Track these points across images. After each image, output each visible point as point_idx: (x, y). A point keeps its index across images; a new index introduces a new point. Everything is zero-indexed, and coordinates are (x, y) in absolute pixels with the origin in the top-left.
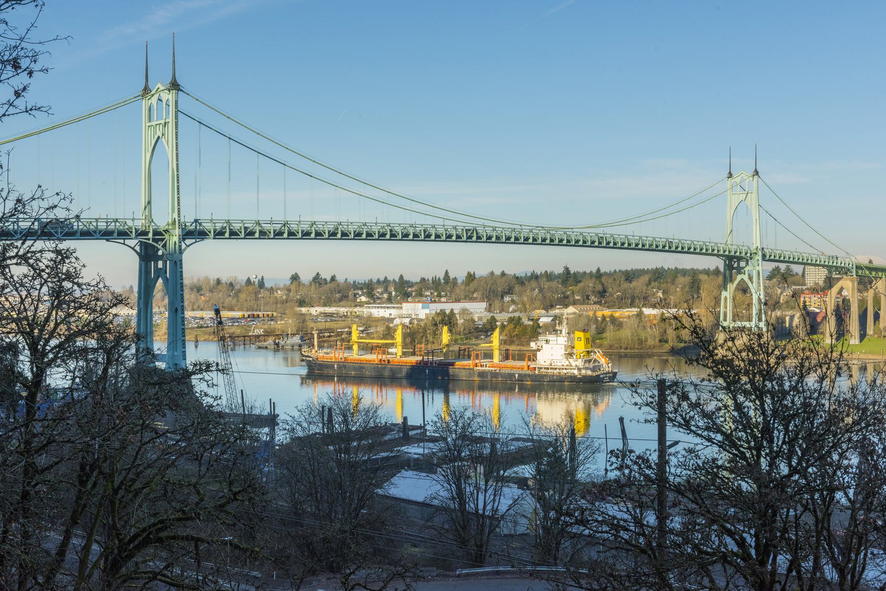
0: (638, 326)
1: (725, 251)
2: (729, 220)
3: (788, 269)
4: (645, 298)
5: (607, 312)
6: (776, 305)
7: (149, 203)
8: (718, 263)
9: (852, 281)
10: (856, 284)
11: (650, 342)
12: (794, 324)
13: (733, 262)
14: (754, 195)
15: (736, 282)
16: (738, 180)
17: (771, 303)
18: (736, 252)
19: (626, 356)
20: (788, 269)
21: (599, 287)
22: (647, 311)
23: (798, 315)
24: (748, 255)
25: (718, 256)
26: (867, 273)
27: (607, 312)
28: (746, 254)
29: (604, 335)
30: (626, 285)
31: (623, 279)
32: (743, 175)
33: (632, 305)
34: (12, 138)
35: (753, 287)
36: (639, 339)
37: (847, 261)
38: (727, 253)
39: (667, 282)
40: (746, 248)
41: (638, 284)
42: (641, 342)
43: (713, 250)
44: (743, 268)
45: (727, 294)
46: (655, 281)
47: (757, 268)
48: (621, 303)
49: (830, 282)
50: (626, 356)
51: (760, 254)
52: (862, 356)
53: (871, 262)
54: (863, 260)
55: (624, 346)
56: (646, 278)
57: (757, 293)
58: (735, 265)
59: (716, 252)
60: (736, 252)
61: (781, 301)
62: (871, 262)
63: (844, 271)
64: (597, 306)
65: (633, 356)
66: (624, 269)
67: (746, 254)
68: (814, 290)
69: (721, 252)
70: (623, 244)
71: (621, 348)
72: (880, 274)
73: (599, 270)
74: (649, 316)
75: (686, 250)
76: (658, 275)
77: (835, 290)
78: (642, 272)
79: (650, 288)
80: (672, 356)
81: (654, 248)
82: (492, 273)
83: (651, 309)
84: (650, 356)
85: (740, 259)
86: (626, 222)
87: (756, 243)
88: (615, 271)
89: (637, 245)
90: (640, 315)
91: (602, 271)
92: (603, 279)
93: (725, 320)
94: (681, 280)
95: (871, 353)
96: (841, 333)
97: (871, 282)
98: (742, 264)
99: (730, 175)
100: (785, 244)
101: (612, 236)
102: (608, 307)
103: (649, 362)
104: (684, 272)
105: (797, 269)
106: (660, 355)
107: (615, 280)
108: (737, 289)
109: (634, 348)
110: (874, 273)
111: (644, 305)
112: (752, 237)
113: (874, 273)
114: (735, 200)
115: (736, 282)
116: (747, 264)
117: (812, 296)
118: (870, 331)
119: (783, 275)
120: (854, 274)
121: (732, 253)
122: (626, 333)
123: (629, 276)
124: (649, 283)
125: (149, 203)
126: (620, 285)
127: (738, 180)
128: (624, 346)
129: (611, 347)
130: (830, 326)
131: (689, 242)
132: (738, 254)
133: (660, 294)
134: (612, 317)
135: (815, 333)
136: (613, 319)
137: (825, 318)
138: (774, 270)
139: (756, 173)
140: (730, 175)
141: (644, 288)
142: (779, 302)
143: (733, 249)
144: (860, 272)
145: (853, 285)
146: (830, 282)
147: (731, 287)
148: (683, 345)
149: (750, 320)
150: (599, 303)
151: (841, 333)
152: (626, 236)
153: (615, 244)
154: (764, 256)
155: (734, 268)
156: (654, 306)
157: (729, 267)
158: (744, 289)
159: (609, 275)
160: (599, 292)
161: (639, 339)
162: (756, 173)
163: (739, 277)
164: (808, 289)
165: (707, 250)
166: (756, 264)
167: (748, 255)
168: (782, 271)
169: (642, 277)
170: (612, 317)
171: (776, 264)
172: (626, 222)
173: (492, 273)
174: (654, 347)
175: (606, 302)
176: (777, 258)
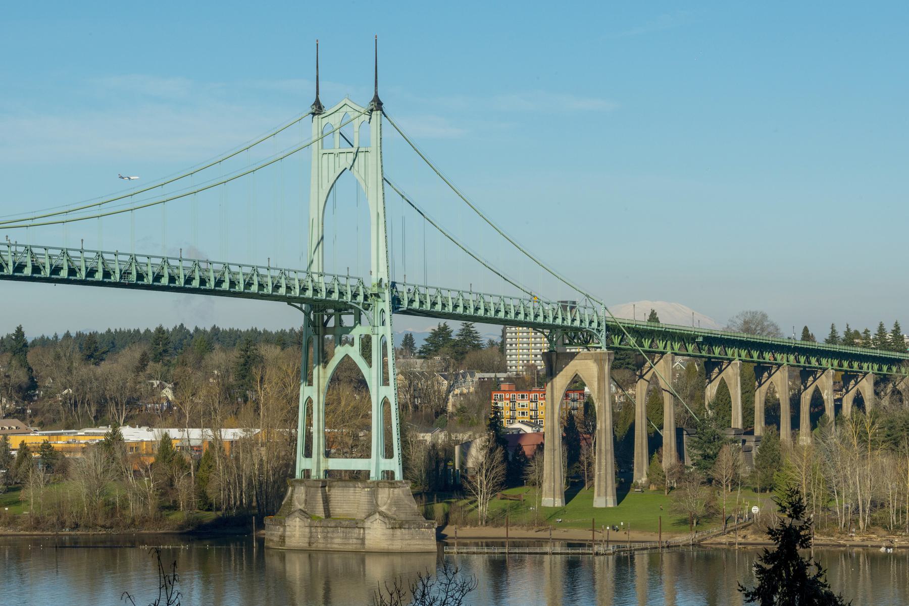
0: (106, 471)
1: (304, 290)
2: (314, 213)
3: (467, 333)
4: (132, 402)
5: (36, 438)
6: (436, 416)
7: (322, 238)
8: (290, 319)
9: (598, 360)
10: (607, 368)
11: (134, 509)
12: (470, 464)
13: (326, 314)
14: (372, 159)
15: (333, 363)
16: (335, 120)
17: (420, 410)
18: (330, 292)
19: (75, 544)
20: (467, 333)
21: (21, 376)
22: (131, 434)
23: (478, 442)
24: (360, 299)
25: (290, 300)
26: (632, 341)
27: (36, 438)
28: (355, 296)
29: (22, 495)
30: (85, 371)
31: (77, 356)
32: (347, 107)
33: (99, 420)
34: (246, 171)
35: (371, 375)
36: (107, 504)
37: (587, 314)
38: (309, 294)
39: (184, 364)
40: (354, 282)
41: (116, 370)
42: (111, 509)
43: (277, 287)
44: (348, 330)
45: (313, 392)
46: (156, 360)
47: (381, 330)
48: (72, 415)
49: (554, 361)
50: (75, 544)
51: (387, 296)
52: (620, 536)
53: (653, 317)
54: (632, 312)
55: (69, 521)
56: (130, 356)
57: (383, 392)
58: (331, 323)
59: (282, 291)
60: (330, 292)
61: (450, 408)
62: (653, 317)
63: (580, 336)
64: (14, 423)
65: (92, 545)
66: (86, 329)
67: (355, 296)
68: (520, 384)
69: (296, 292)
70: (56, 270)
71: (63, 525)
72: (661, 345)
73: (20, 333)
74: (138, 444)
75: (240, 287)
76: (164, 347)
77: (561, 381)
78: (133, 337)
79: (142, 377)
80: (189, 541)
81: (158, 283)
82: (109, 331)
83: (144, 429)
84: (133, 543)
85: (341, 308)
86: (64, 217)
87: (377, 271)
88: (67, 335)
89: (91, 272)
90: (115, 438)
91: (30, 337)
92: (30, 358)
93: (308, 454)
94: (219, 357)
95: (635, 527)
96: (576, 482)
97: (640, 365)
98: (348, 320)
99: (318, 109)
100: (450, 273)
101: (28, 249)
102: (42, 425)
103: (132, 555)
104: (216, 338)
105: (487, 333)
106: (156, 540)
107: (58, 357)
108: (335, 379)
109: (94, 526)
110: (647, 343)
111: (130, 421)
112: (368, 258)
113: (647, 343)
114: (329, 168)
115: (333, 363)
116: (358, 320)
117: (518, 395)
118: (641, 477)
119: (456, 344)
120: (603, 344)
121: (323, 295)
122: (75, 489)
123: (94, 348)
124: (142, 365)
125: (322, 238)
126: (70, 370)
127: (335, 120)
128: (69, 521)
129: (38, 523)
130: (552, 467)
131: (248, 270)
132: (335, 296)
133: (168, 393)
134: (46, 448)
135: (520, 483)
136: (50, 456)
137: (540, 447)
138: (435, 334)
139: (377, 104)
140: (318, 109)
141: (130, 376)
142: (444, 411)
143: (323, 283)
144: (616, 341)
145: (601, 369)
146: (554, 361)
147: (322, 375)
148: (211, 516)
149: (366, 454)
150: (19, 414)
151: (576, 482)
152: (65, 252)
153: (36, 269)
154: (396, 302)
155: (326, 330)
156: (149, 423)
157: (316, 327)
158: (350, 379)
159: (43, 343)
160: (20, 389)
161: (107, 504)
162: (377, 104)
163: (340, 352)
164: (508, 379)
165: (261, 286)
166: (377, 322)
167: (360, 299)
168: (454, 337)
169: (125, 351)
170: (46, 448)
171: (442, 321)
172: (64, 217)
173: (109, 331)
174: (144, 521)
175: (35, 413)
176: (427, 307)
